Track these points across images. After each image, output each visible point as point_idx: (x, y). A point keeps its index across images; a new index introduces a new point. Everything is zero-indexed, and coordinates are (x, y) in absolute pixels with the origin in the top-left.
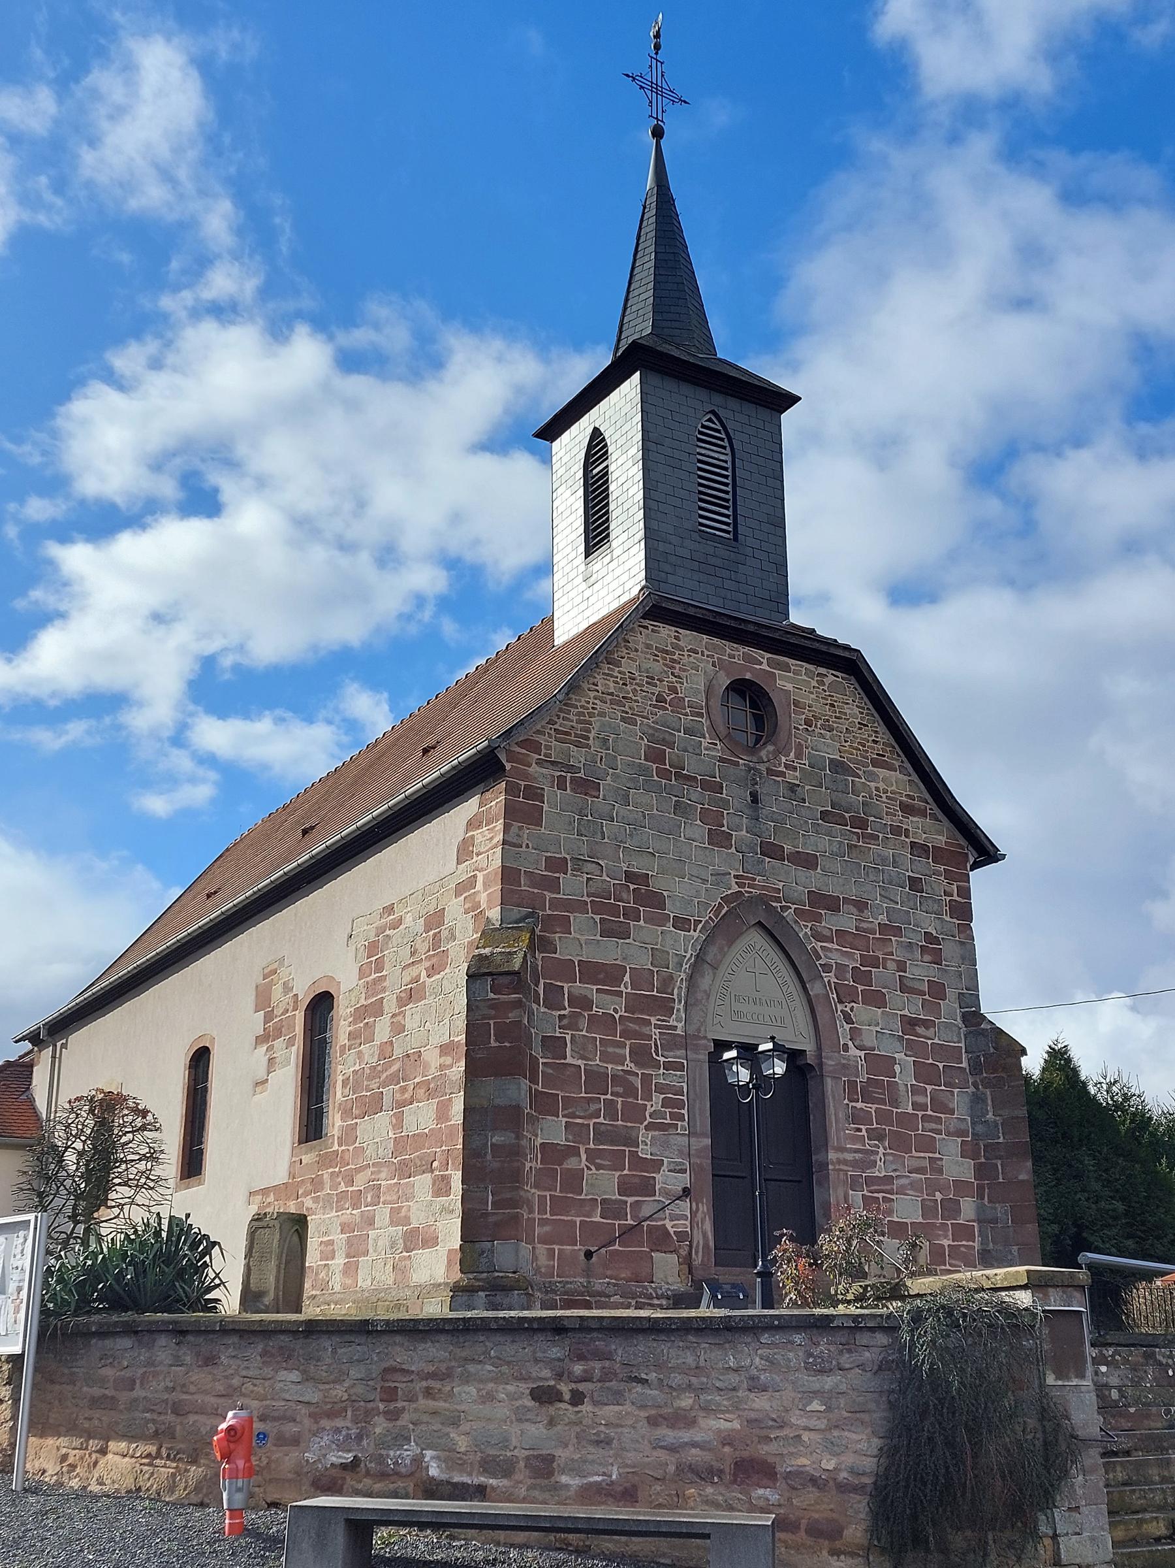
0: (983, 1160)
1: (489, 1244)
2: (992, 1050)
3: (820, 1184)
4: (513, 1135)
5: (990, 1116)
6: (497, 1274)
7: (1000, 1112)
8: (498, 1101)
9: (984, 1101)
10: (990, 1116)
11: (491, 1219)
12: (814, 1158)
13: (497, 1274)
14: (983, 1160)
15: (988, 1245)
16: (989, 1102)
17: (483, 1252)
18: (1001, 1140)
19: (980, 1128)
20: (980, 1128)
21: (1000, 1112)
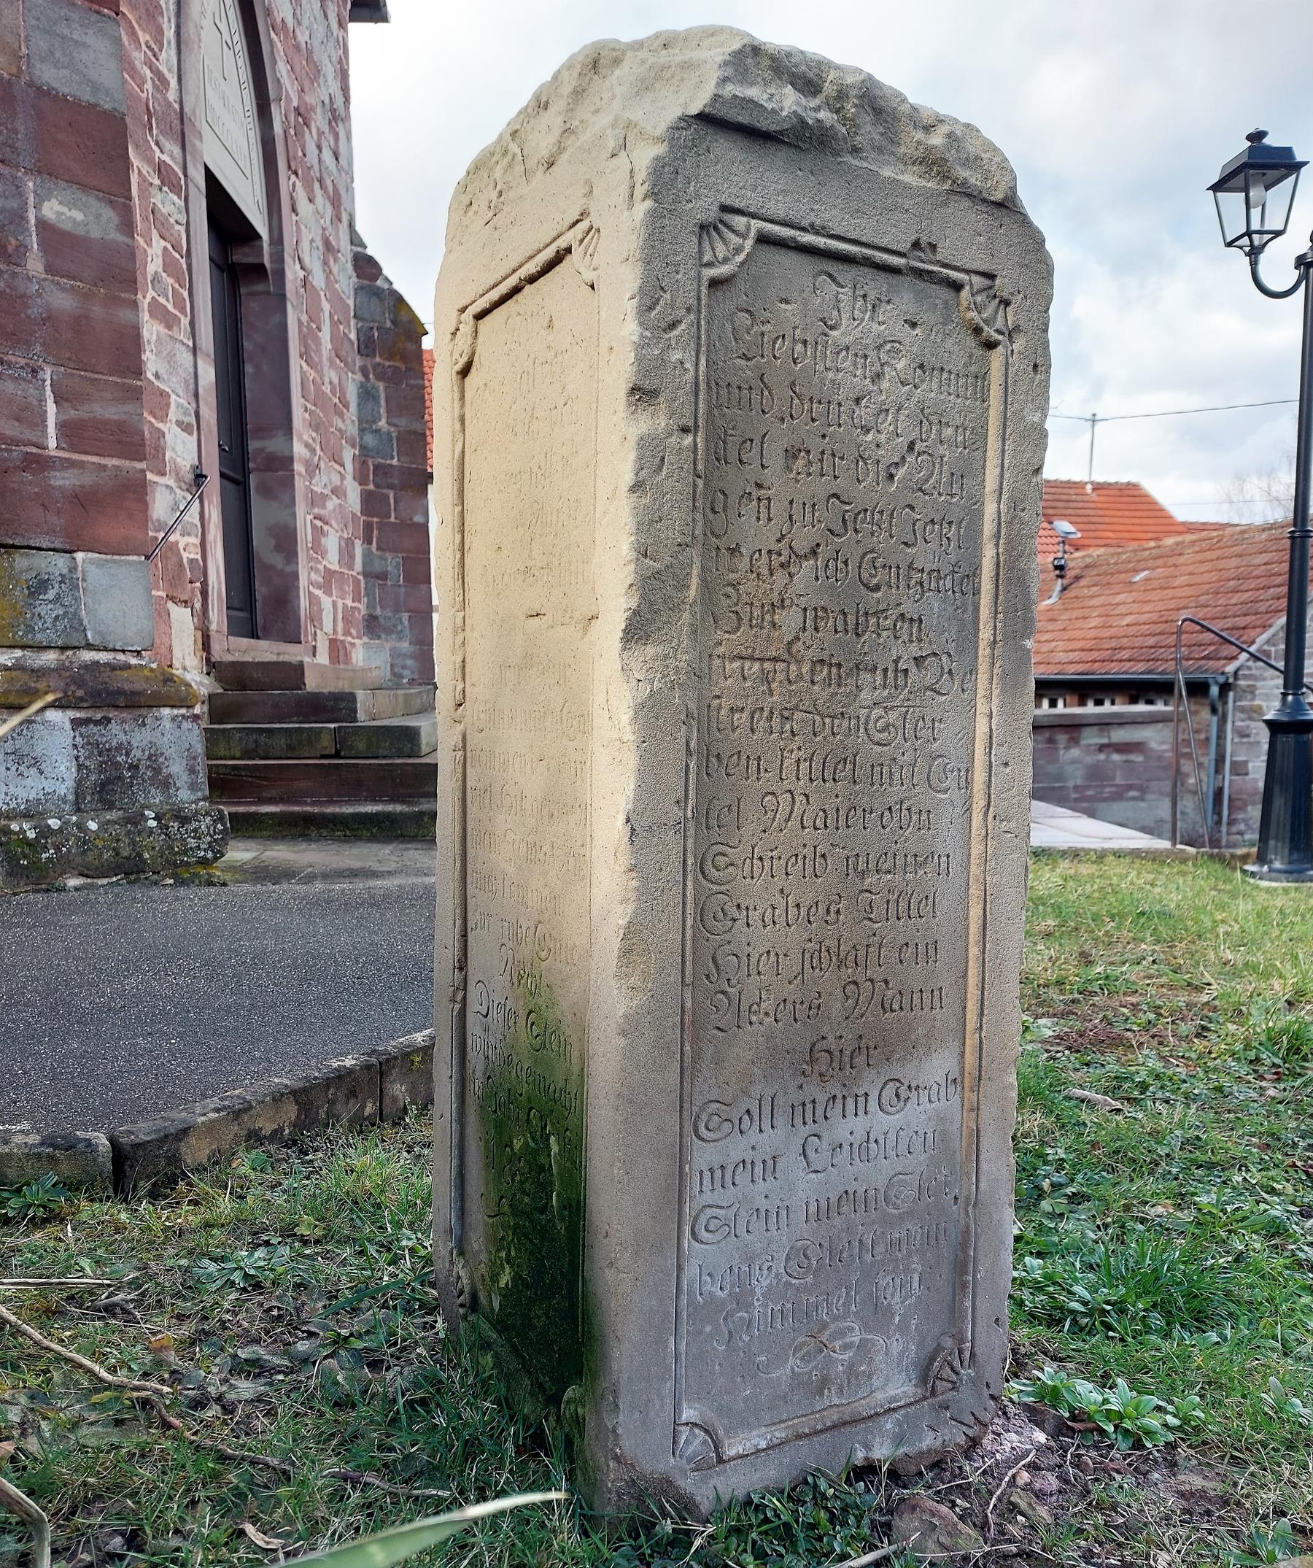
0: (371, 487)
1: (59, 563)
2: (389, 324)
3: (266, 492)
4: (109, 214)
5: (382, 423)
6: (87, 656)
7: (395, 421)
8: (48, 75)
9: (375, 399)
10: (382, 423)
11: (62, 480)
12: (253, 445)
13: (87, 656)
14: (371, 487)
15: (374, 608)
16: (383, 402)
17: (43, 585)
18: (395, 462)
19: (370, 440)
20: (370, 440)
21: (395, 421)
